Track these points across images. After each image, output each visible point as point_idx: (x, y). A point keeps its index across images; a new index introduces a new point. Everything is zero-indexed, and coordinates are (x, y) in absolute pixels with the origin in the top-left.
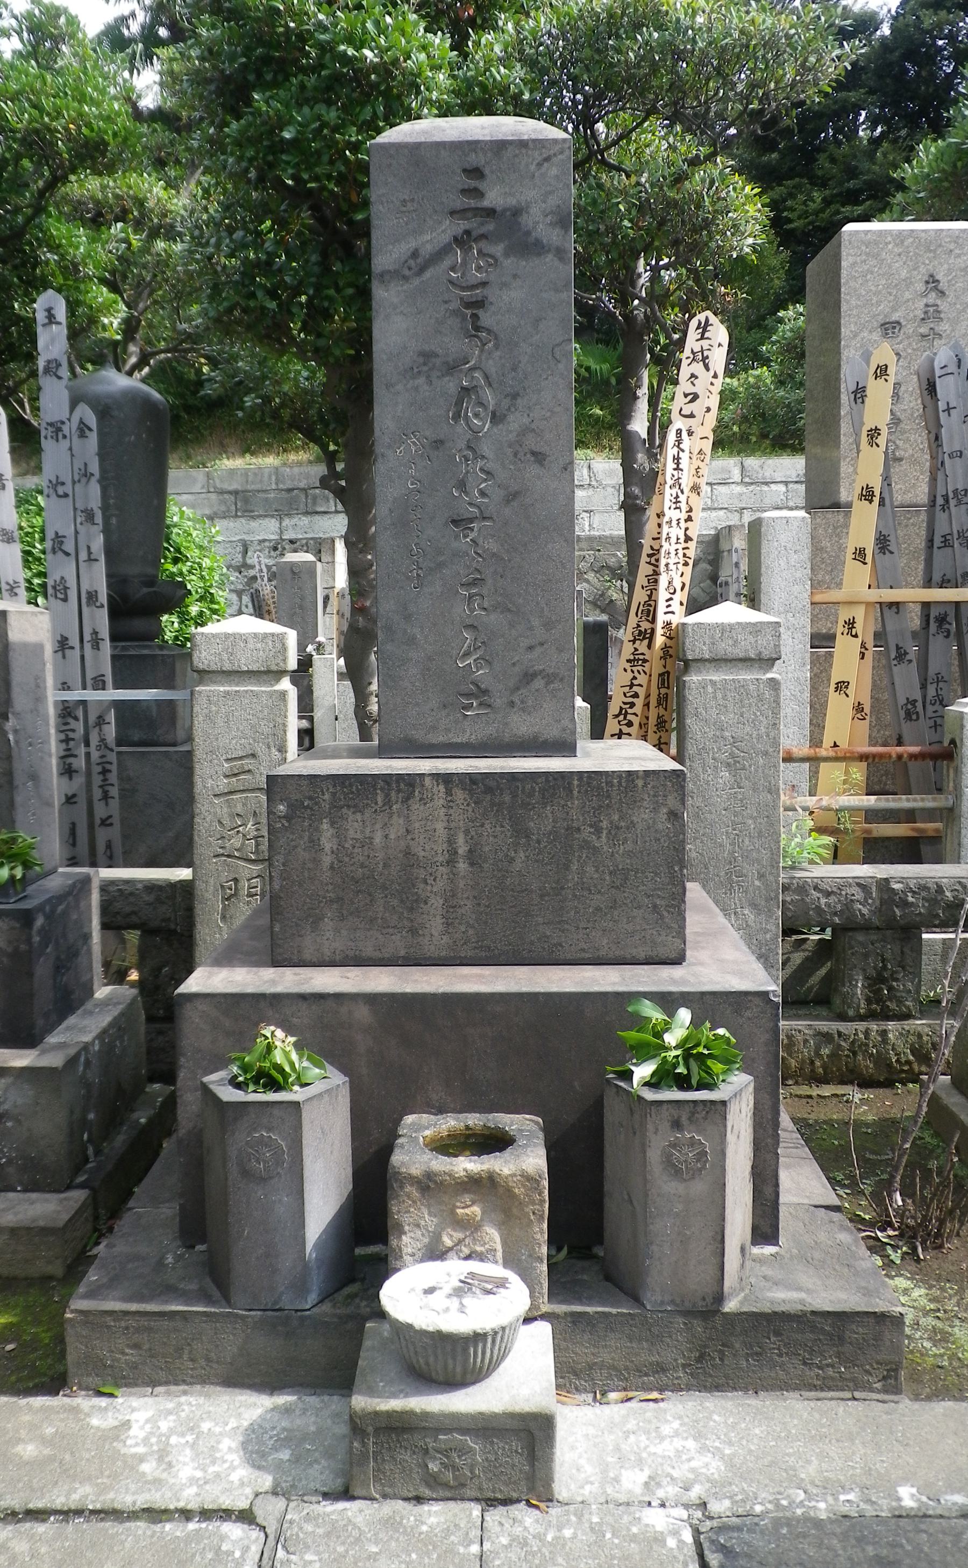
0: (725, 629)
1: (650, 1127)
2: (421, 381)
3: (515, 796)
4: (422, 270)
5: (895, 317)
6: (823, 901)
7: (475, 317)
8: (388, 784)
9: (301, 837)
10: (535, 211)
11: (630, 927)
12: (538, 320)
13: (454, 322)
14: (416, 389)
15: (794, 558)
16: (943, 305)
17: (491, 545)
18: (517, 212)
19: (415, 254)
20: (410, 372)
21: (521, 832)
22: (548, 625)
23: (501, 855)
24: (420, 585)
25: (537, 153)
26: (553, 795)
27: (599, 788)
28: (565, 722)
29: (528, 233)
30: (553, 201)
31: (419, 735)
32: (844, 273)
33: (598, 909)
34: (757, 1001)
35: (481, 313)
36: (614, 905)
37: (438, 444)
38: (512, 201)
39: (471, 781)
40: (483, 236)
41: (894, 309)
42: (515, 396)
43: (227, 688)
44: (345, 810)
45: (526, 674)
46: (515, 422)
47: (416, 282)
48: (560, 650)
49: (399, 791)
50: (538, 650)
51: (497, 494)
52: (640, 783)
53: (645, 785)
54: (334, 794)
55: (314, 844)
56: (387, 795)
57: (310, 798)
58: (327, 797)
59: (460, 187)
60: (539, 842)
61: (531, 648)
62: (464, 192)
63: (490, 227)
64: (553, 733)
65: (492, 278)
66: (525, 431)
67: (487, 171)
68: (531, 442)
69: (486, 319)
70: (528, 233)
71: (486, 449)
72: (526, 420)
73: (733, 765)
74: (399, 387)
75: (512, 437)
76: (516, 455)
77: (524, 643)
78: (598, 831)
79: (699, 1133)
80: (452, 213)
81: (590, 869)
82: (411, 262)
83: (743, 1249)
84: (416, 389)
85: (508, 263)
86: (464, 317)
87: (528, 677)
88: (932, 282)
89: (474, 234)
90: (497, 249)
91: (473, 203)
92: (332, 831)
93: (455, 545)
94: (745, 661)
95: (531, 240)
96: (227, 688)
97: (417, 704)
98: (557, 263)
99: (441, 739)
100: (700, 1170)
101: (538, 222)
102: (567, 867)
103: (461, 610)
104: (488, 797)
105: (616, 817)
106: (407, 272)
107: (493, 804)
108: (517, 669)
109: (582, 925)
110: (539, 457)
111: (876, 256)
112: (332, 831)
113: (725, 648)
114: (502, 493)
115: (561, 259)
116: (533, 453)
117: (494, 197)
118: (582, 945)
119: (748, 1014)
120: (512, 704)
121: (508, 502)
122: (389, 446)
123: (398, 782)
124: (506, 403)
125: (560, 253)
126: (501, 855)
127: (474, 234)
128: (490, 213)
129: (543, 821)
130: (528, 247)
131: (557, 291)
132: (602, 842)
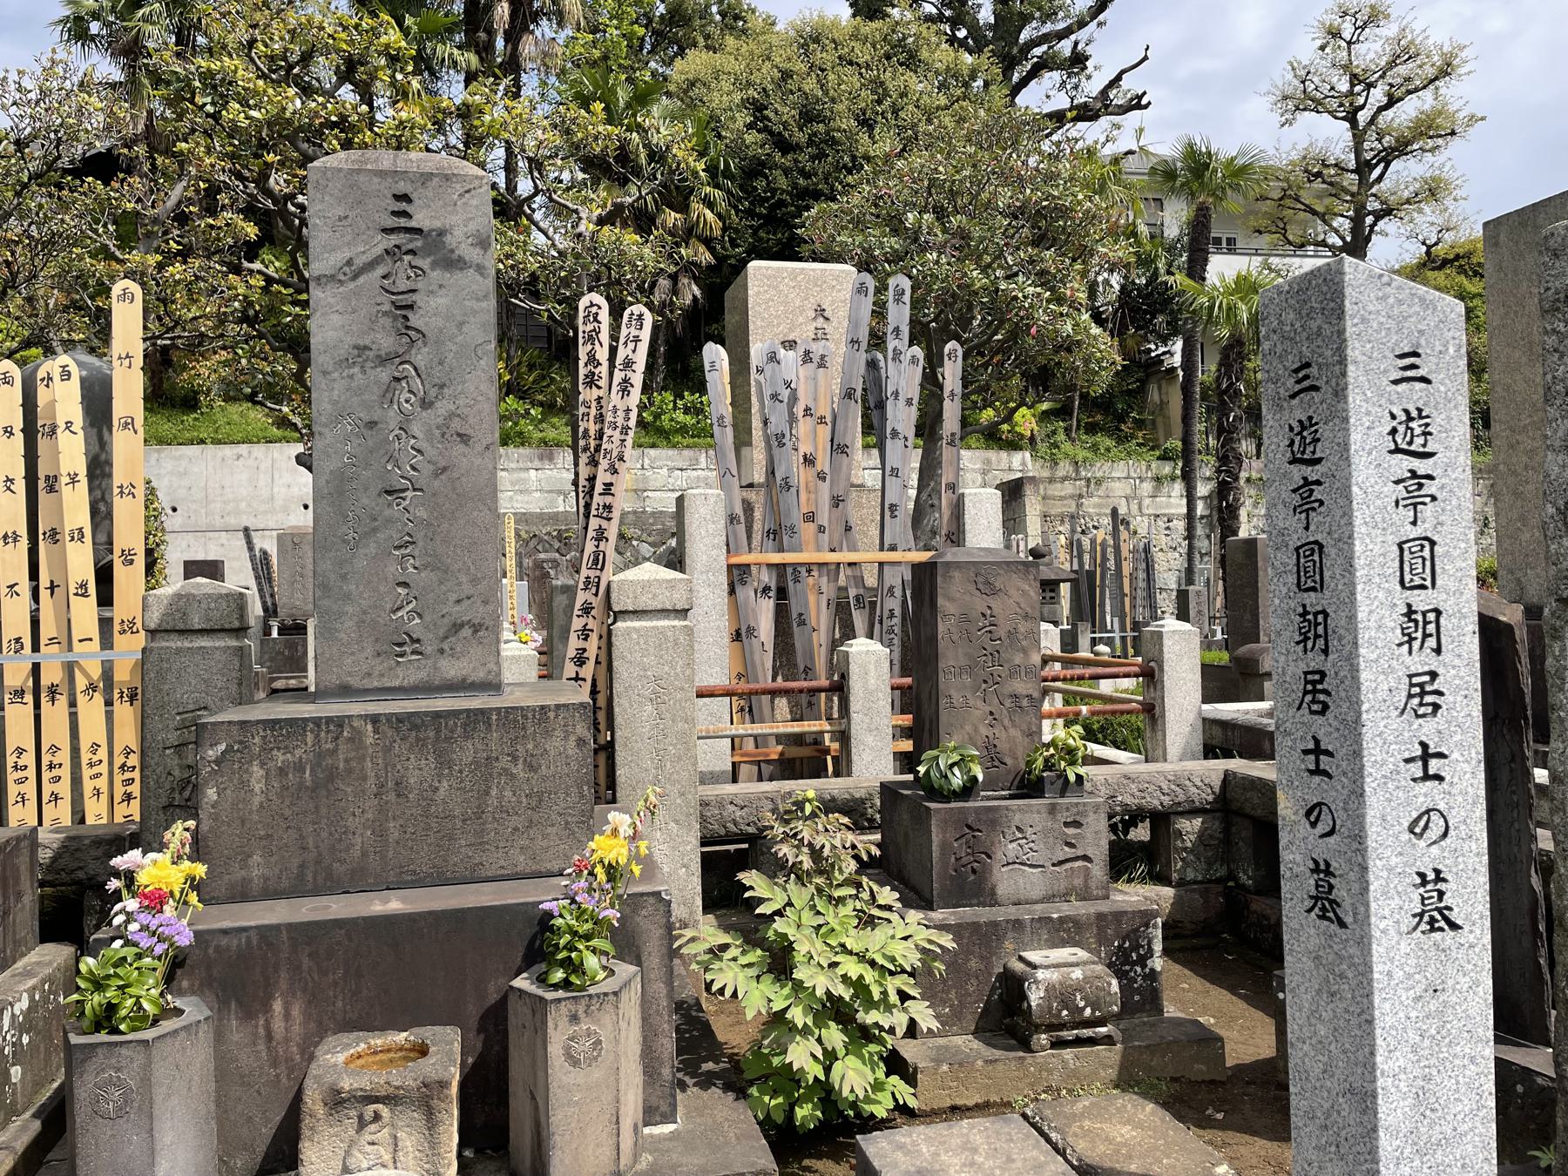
0: (646, 585)
1: (550, 1024)
2: (356, 370)
3: (438, 731)
4: (355, 277)
5: (791, 338)
6: (738, 814)
7: (406, 318)
8: (319, 726)
9: (231, 780)
10: (458, 232)
11: (545, 844)
12: (461, 324)
13: (387, 321)
14: (351, 377)
15: (711, 526)
16: (829, 329)
17: (422, 513)
18: (442, 233)
19: (349, 263)
20: (345, 363)
21: (444, 763)
22: (474, 581)
23: (425, 785)
24: (357, 546)
25: (458, 186)
26: (474, 729)
27: (516, 721)
28: (492, 666)
29: (452, 251)
30: (472, 227)
31: (355, 682)
32: (751, 301)
33: (516, 829)
34: (651, 900)
35: (410, 315)
36: (531, 824)
37: (372, 424)
38: (437, 224)
39: (400, 719)
40: (412, 252)
41: (791, 330)
42: (442, 386)
43: (179, 644)
44: (275, 752)
45: (455, 625)
46: (443, 407)
47: (352, 285)
48: (485, 602)
49: (328, 732)
50: (466, 603)
51: (427, 469)
52: (552, 715)
53: (557, 716)
54: (264, 738)
55: (244, 784)
56: (317, 736)
57: (240, 742)
58: (257, 740)
59: (391, 209)
60: (461, 772)
61: (458, 601)
62: (394, 213)
63: (418, 243)
64: (479, 675)
65: (420, 286)
66: (452, 415)
67: (414, 196)
68: (456, 424)
69: (415, 320)
70: (452, 251)
71: (415, 429)
72: (452, 407)
73: (656, 699)
74: (336, 375)
75: (440, 420)
76: (443, 435)
77: (454, 597)
78: (515, 759)
79: (594, 1023)
80: (385, 230)
81: (508, 793)
82: (346, 269)
83: (636, 1126)
84: (351, 377)
85: (435, 275)
86: (395, 318)
87: (457, 627)
88: (820, 312)
89: (404, 249)
90: (425, 263)
91: (403, 222)
92: (262, 772)
93: (387, 512)
94: (664, 612)
95: (455, 256)
96: (179, 644)
97: (353, 654)
98: (478, 277)
99: (376, 684)
100: (595, 1059)
101: (460, 242)
102: (487, 793)
103: (393, 569)
104: (414, 734)
105: (530, 746)
106: (342, 277)
107: (418, 739)
108: (446, 620)
109: (502, 844)
110: (464, 438)
111: (776, 288)
112: (262, 772)
113: (645, 602)
114: (432, 467)
115: (482, 274)
116: (459, 435)
117: (420, 219)
118: (502, 863)
119: (644, 912)
120: (442, 651)
121: (437, 475)
122: (326, 426)
123: (327, 723)
124: (433, 392)
125: (480, 269)
126: (425, 785)
127: (404, 249)
128: (419, 231)
129: (466, 752)
130: (452, 263)
131: (478, 300)
132: (519, 769)
